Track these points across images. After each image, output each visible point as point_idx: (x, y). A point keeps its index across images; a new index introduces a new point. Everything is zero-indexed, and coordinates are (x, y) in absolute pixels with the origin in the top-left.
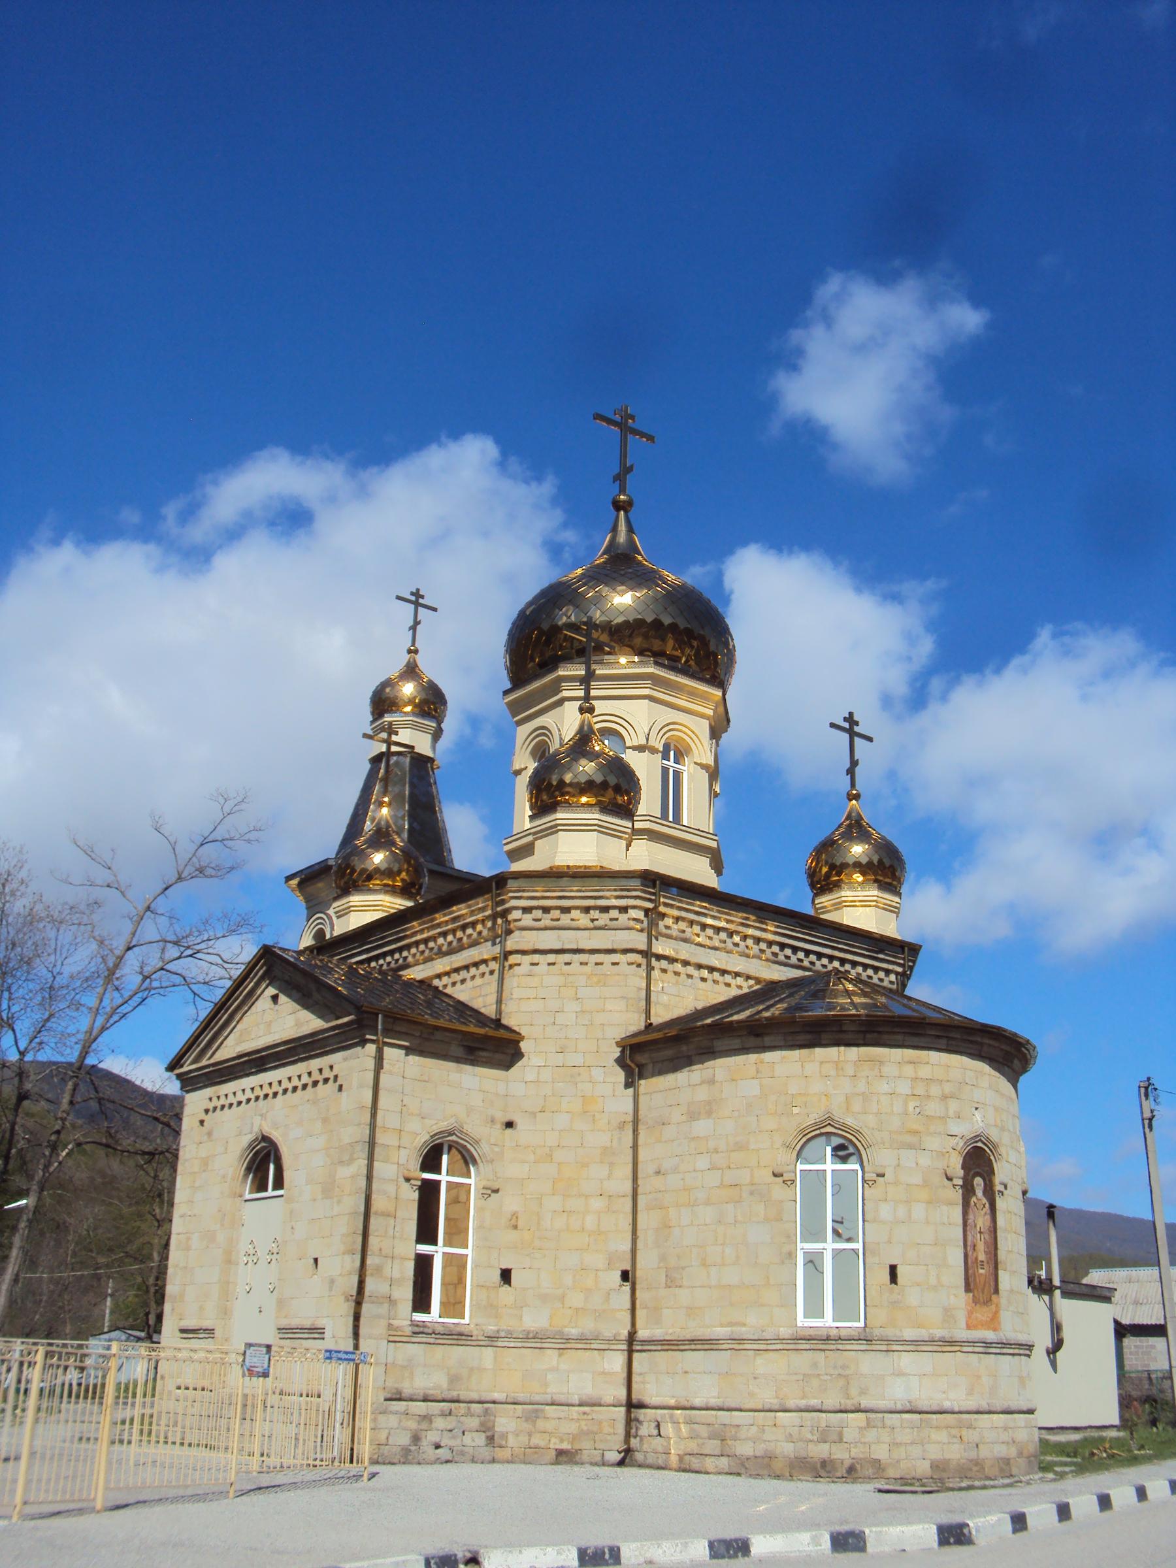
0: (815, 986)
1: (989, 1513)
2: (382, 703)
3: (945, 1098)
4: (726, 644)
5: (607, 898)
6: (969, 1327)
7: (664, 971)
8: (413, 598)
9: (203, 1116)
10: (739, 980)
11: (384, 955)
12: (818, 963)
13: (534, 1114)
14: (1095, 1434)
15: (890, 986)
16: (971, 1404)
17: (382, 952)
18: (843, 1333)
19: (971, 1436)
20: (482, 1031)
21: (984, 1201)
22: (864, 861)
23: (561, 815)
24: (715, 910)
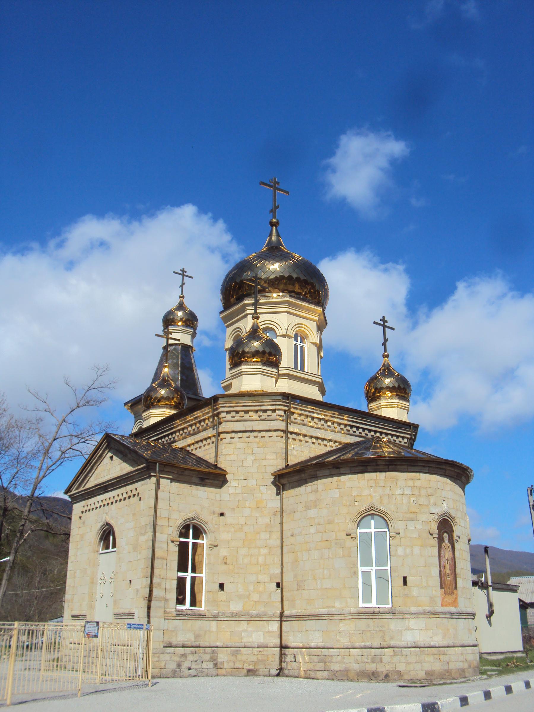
0: (365, 444)
1: (449, 697)
2: (168, 321)
3: (428, 495)
4: (324, 286)
5: (266, 406)
6: (442, 606)
7: (294, 439)
8: (181, 272)
9: (81, 515)
10: (331, 443)
11: (165, 437)
12: (369, 434)
13: (234, 509)
14: (510, 655)
15: (405, 444)
16: (445, 643)
17: (164, 435)
18: (382, 610)
19: (445, 658)
20: (207, 470)
21: (449, 545)
22: (391, 386)
24: (318, 410)
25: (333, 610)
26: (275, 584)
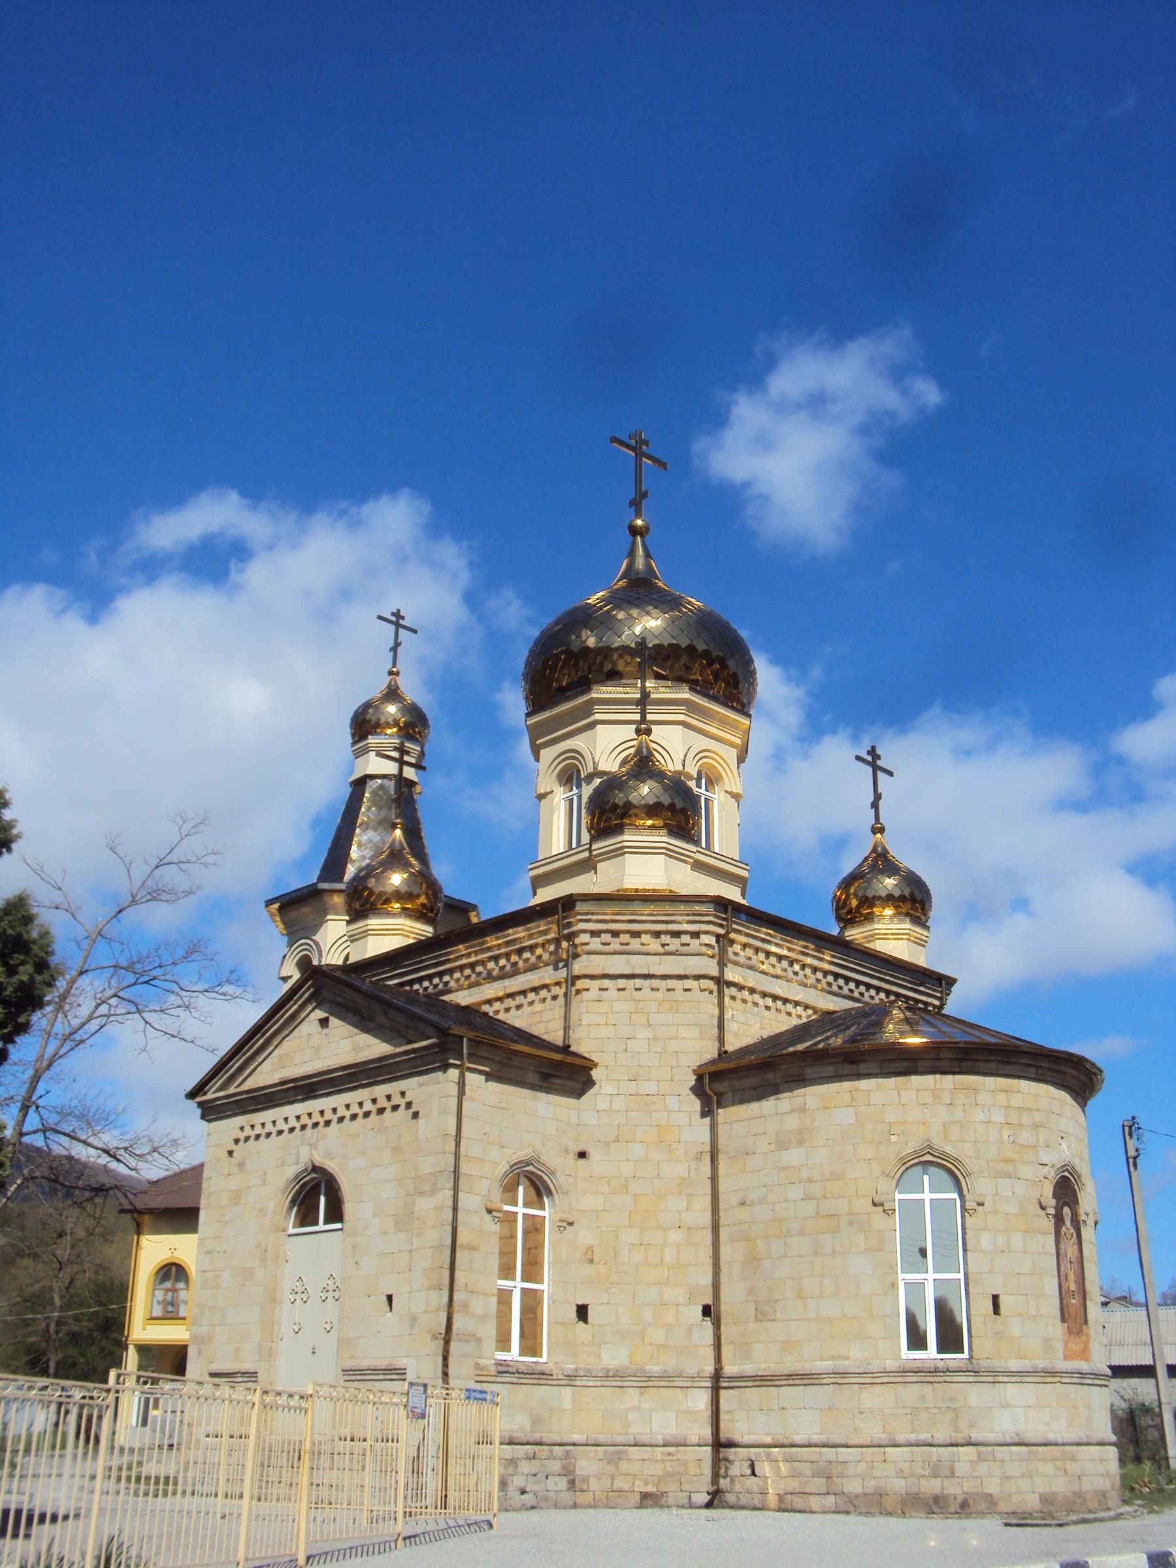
0: (874, 1017)
2: (363, 726)
3: (1035, 1127)
5: (680, 923)
6: (1066, 1358)
8: (394, 619)
9: (233, 1147)
12: (866, 994)
13: (608, 1144)
16: (1072, 1436)
21: (1072, 1230)
23: (628, 837)
24: (778, 938)
25: (843, 1365)
26: (701, 1308)
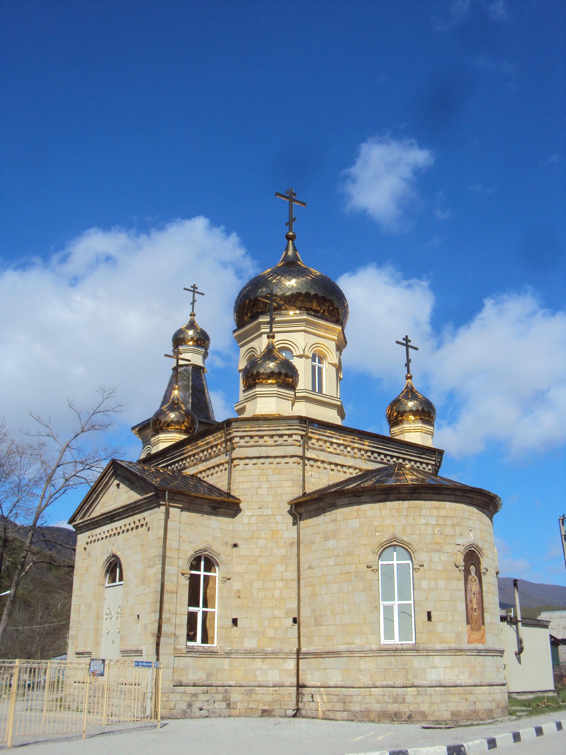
0: (387, 471)
1: (476, 739)
2: (178, 340)
3: (454, 525)
4: (343, 303)
5: (282, 430)
6: (469, 642)
7: (312, 466)
8: (192, 289)
9: (85, 546)
10: (351, 470)
11: (174, 463)
12: (391, 461)
13: (248, 540)
14: (541, 695)
15: (429, 471)
16: (471, 682)
17: (174, 461)
18: (404, 647)
19: (472, 698)
20: (219, 499)
21: (476, 577)
22: (414, 409)
24: (337, 435)
25: (353, 647)
26: (292, 619)
